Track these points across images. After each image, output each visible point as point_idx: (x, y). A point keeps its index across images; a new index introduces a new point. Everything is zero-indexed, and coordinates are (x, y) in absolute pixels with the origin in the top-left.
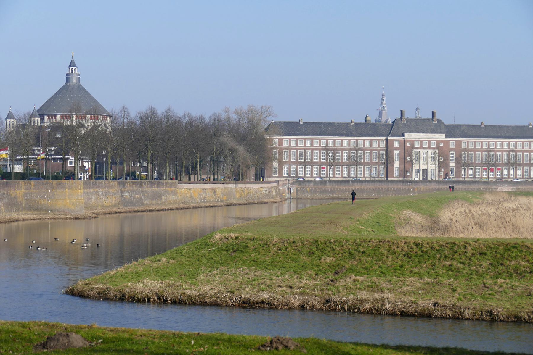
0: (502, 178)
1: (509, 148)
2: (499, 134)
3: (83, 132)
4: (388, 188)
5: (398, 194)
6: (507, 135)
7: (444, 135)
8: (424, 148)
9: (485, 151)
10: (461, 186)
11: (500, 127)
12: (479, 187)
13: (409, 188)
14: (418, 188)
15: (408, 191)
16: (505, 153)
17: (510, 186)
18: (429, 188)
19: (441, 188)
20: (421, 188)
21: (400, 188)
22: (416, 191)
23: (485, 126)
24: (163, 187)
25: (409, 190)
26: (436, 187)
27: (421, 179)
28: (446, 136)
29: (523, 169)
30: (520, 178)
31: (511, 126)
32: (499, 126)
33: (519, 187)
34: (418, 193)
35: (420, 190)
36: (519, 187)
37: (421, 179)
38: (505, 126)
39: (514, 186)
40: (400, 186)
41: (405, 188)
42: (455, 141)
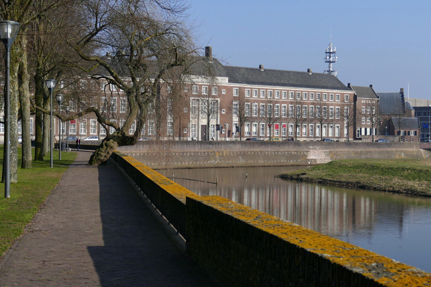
0: (78, 134)
1: (266, 98)
2: (282, 81)
3: (138, 80)
4: (183, 153)
5: (196, 161)
6: (291, 82)
7: (227, 79)
8: (204, 96)
9: (263, 102)
10: (269, 149)
11: (281, 73)
12: (290, 150)
13: (208, 152)
14: (219, 153)
15: (208, 157)
16: (261, 104)
17: (322, 148)
18: (233, 152)
19: (247, 152)
20: (223, 152)
21: (198, 153)
22: (217, 157)
23: (265, 70)
24: (413, 152)
25: (209, 155)
26: (241, 150)
27: (200, 140)
28: (230, 81)
29: (259, 124)
30: (332, 137)
31: (291, 72)
32: (279, 71)
33: (331, 150)
34: (221, 160)
35: (222, 156)
36: (331, 150)
37: (200, 140)
38: (285, 72)
39: (326, 148)
40: (197, 149)
41: (204, 153)
42: (240, 88)
